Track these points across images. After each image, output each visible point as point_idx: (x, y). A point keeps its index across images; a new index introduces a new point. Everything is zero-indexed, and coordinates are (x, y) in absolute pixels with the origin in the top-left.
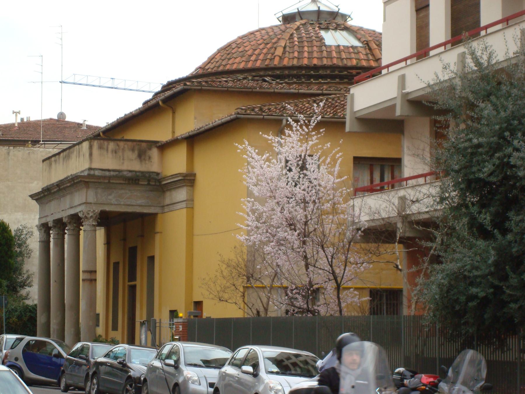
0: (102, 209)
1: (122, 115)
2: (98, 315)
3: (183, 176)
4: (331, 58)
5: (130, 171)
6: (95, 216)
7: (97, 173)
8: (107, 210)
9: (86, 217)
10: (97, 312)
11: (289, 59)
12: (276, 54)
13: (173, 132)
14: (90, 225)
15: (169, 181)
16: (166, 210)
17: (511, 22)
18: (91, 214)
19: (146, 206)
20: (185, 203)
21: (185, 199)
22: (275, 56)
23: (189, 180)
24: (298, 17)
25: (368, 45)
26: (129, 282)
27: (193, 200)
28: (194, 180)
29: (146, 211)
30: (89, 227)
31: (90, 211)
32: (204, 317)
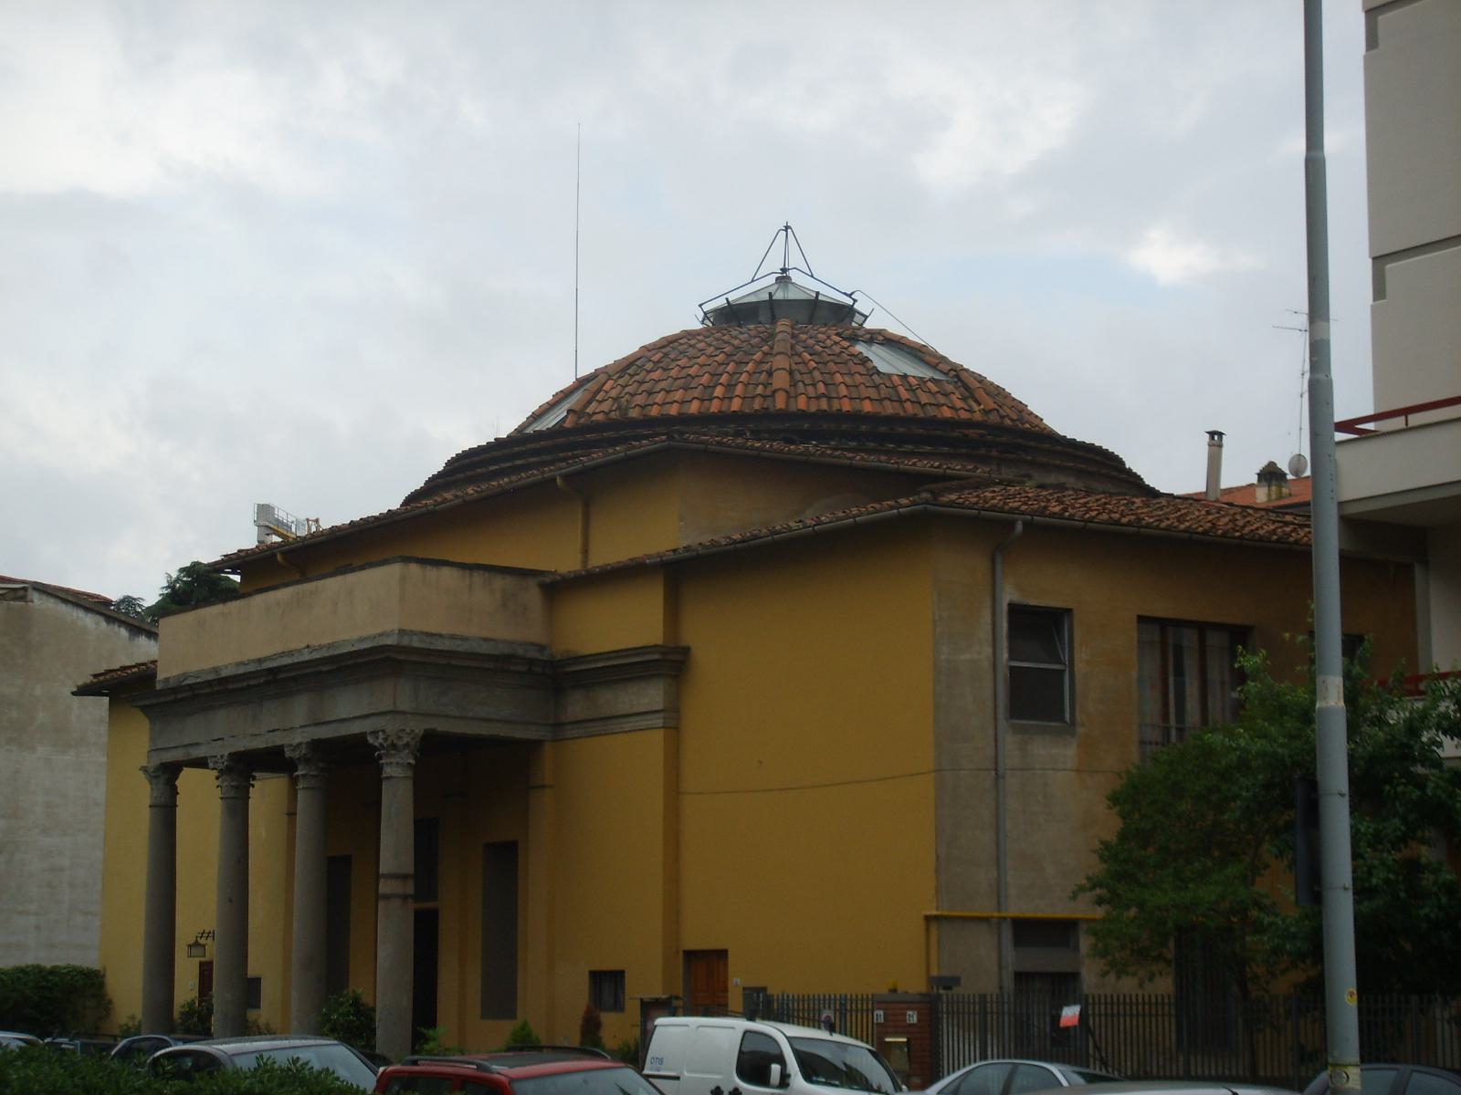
0: (427, 727)
1: (97, 593)
2: (257, 981)
3: (662, 653)
4: (900, 401)
5: (485, 640)
7: (416, 643)
8: (439, 729)
9: (394, 746)
10: (252, 971)
12: (775, 386)
13: (585, 552)
14: (403, 765)
20: (661, 715)
21: (660, 707)
22: (775, 391)
23: (670, 663)
24: (764, 315)
25: (960, 379)
29: (519, 733)
30: (399, 770)
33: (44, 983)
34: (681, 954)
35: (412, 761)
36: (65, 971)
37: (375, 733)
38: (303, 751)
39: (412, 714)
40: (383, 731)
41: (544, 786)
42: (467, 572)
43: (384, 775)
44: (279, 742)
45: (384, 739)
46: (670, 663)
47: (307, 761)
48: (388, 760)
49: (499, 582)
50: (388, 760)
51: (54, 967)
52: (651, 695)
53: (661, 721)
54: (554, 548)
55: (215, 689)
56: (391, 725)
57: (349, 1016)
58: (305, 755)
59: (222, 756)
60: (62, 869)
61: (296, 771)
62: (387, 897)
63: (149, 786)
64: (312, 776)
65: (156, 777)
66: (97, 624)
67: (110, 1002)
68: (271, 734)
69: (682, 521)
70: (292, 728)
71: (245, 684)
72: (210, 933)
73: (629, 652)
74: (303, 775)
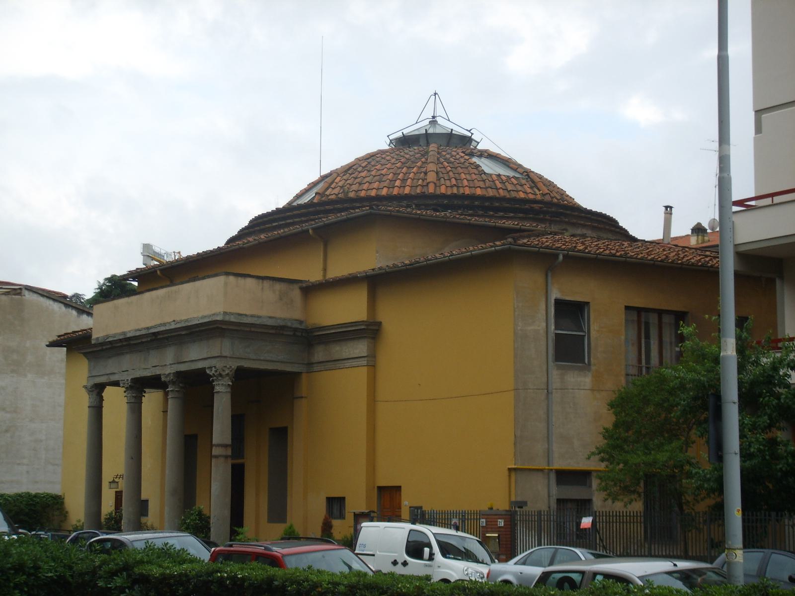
3: (366, 325)
6: (233, 371)
9: (220, 375)
11: (447, 187)
12: (428, 180)
13: (325, 270)
14: (225, 385)
15: (329, 332)
16: (315, 369)
17: (304, 191)
19: (287, 362)
20: (366, 359)
21: (365, 355)
22: (428, 183)
23: (370, 331)
24: (423, 142)
25: (529, 177)
27: (375, 357)
28: (377, 330)
29: (289, 368)
31: (226, 366)
32: (581, 527)
33: (31, 502)
35: (230, 383)
37: (210, 368)
38: (172, 378)
39: (230, 357)
41: (302, 397)
42: (261, 281)
44: (158, 373)
45: (215, 371)
46: (370, 331)
47: (173, 383)
49: (278, 286)
52: (360, 348)
54: (309, 269)
56: (219, 364)
58: (172, 379)
59: (127, 380)
60: (41, 441)
61: (168, 388)
62: (216, 457)
64: (176, 391)
66: (60, 308)
67: (67, 512)
69: (377, 253)
70: (166, 365)
71: (140, 341)
72: (120, 476)
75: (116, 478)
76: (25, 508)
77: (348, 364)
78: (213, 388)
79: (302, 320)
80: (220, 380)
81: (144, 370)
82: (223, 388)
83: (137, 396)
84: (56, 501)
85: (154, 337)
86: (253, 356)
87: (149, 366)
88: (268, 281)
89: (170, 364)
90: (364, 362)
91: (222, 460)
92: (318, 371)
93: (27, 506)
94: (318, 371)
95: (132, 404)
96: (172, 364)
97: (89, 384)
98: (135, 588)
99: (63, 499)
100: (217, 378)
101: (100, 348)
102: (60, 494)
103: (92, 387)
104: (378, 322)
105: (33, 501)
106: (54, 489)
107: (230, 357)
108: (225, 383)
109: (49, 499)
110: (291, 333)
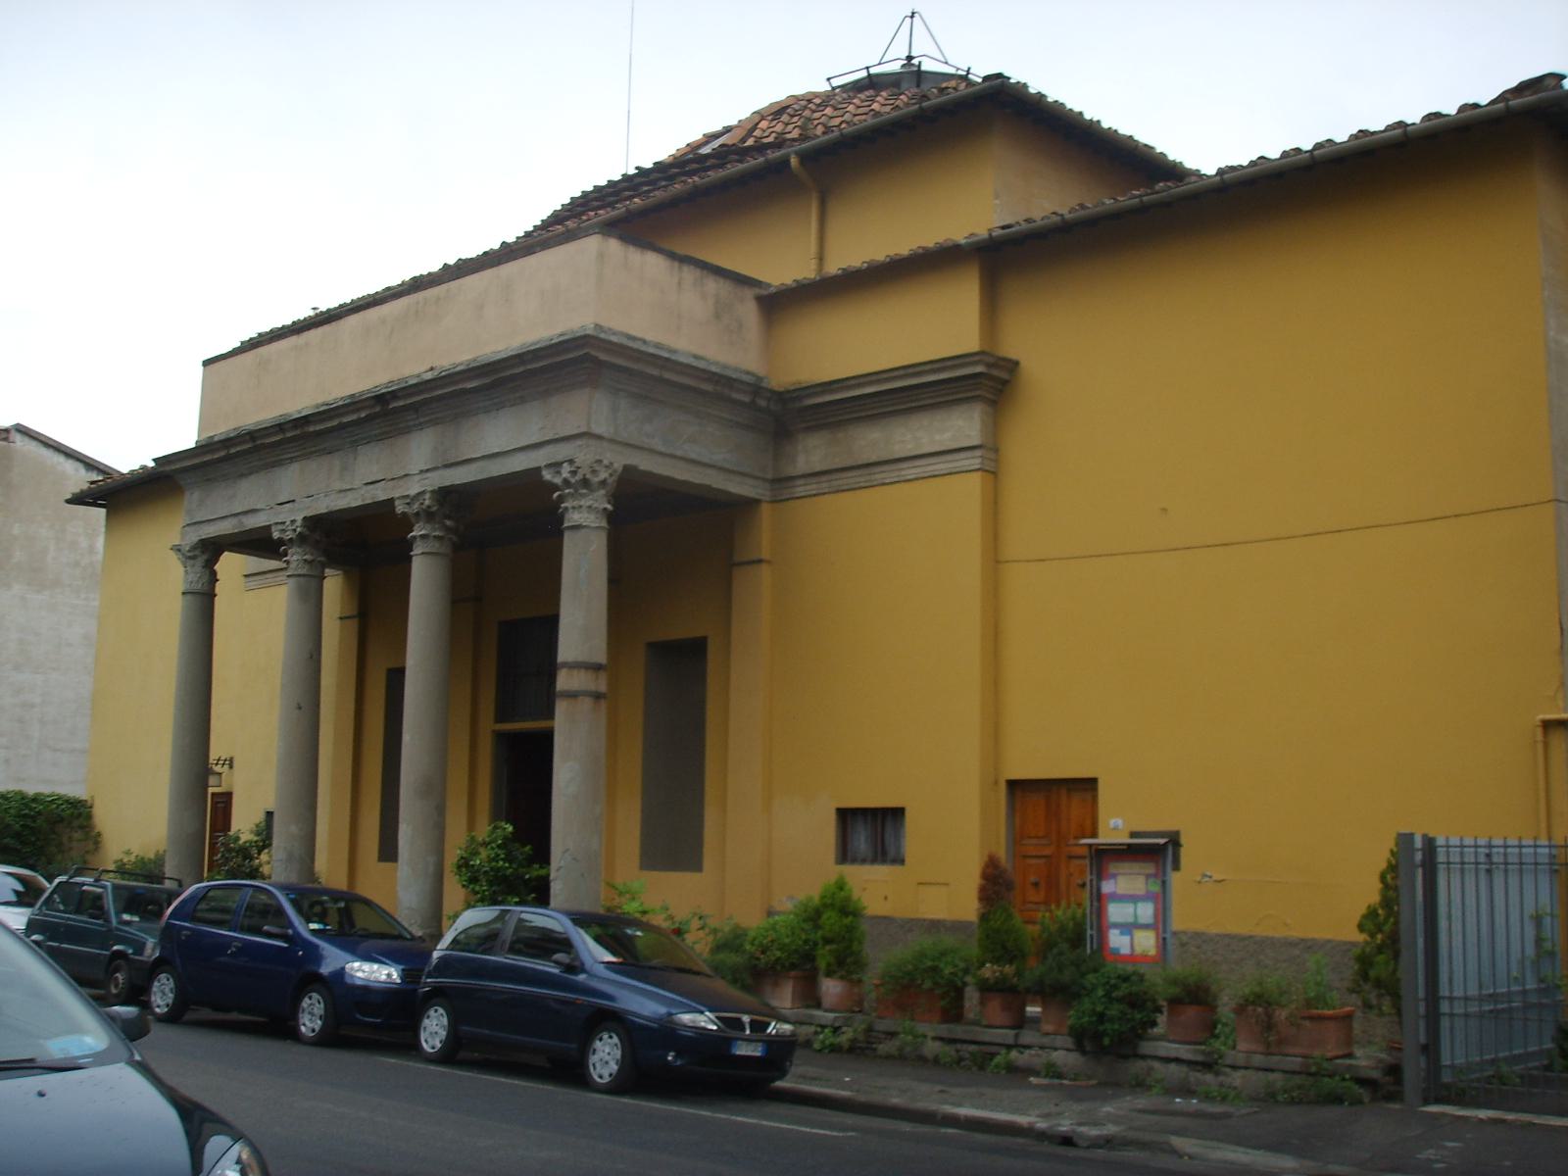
0: (629, 462)
1: (1143, 137)
3: (989, 365)
6: (614, 478)
9: (585, 483)
13: (820, 259)
16: (800, 491)
18: (603, 475)
21: (976, 442)
23: (987, 383)
26: (499, 719)
27: (996, 450)
28: (1005, 383)
33: (27, 811)
34: (1003, 787)
35: (609, 507)
36: (51, 799)
37: (556, 466)
38: (427, 502)
40: (571, 462)
41: (760, 561)
42: (676, 264)
43: (565, 525)
44: (382, 496)
45: (571, 472)
46: (987, 383)
47: (429, 516)
48: (576, 503)
49: (713, 285)
50: (576, 503)
51: (37, 794)
52: (963, 426)
53: (978, 461)
54: (782, 254)
55: (289, 435)
56: (584, 455)
57: (497, 862)
58: (429, 507)
59: (293, 522)
60: (33, 706)
61: (412, 531)
62: (572, 695)
63: (182, 569)
64: (435, 537)
65: (190, 558)
66: (77, 470)
67: (99, 834)
68: (372, 486)
69: (996, 198)
70: (406, 475)
71: (335, 423)
72: (225, 760)
73: (896, 373)
74: (423, 537)
75: (217, 764)
76: (13, 823)
77: (910, 471)
78: (561, 519)
79: (760, 375)
80: (583, 496)
81: (342, 495)
82: (592, 517)
83: (313, 561)
84: (76, 811)
85: (378, 409)
86: (657, 444)
87: (357, 483)
88: (692, 267)
89: (421, 471)
90: (972, 461)
91: (586, 703)
92: (810, 496)
93: (18, 820)
94: (810, 496)
95: (301, 579)
96: (427, 471)
97: (189, 542)
98: (319, 1022)
99: (91, 807)
100: (576, 491)
101: (222, 453)
102: (84, 798)
103: (194, 548)
104: (1010, 361)
105: (31, 809)
106: (72, 789)
107: (612, 441)
108: (595, 505)
109: (63, 806)
110: (746, 399)
